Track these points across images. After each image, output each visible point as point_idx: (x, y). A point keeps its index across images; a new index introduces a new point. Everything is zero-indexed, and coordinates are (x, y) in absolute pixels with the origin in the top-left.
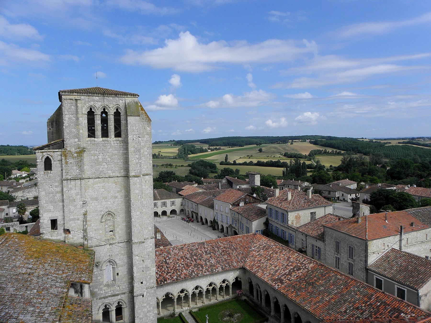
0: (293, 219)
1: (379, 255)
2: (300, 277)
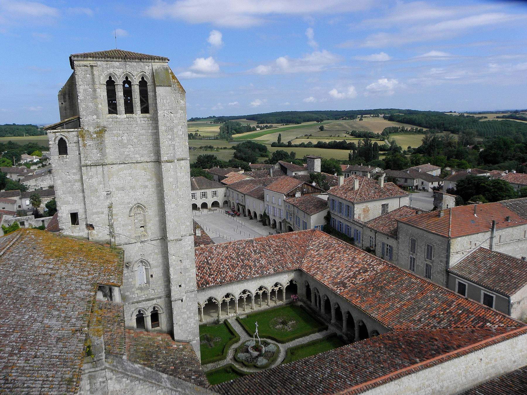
0: (360, 212)
2: (367, 280)
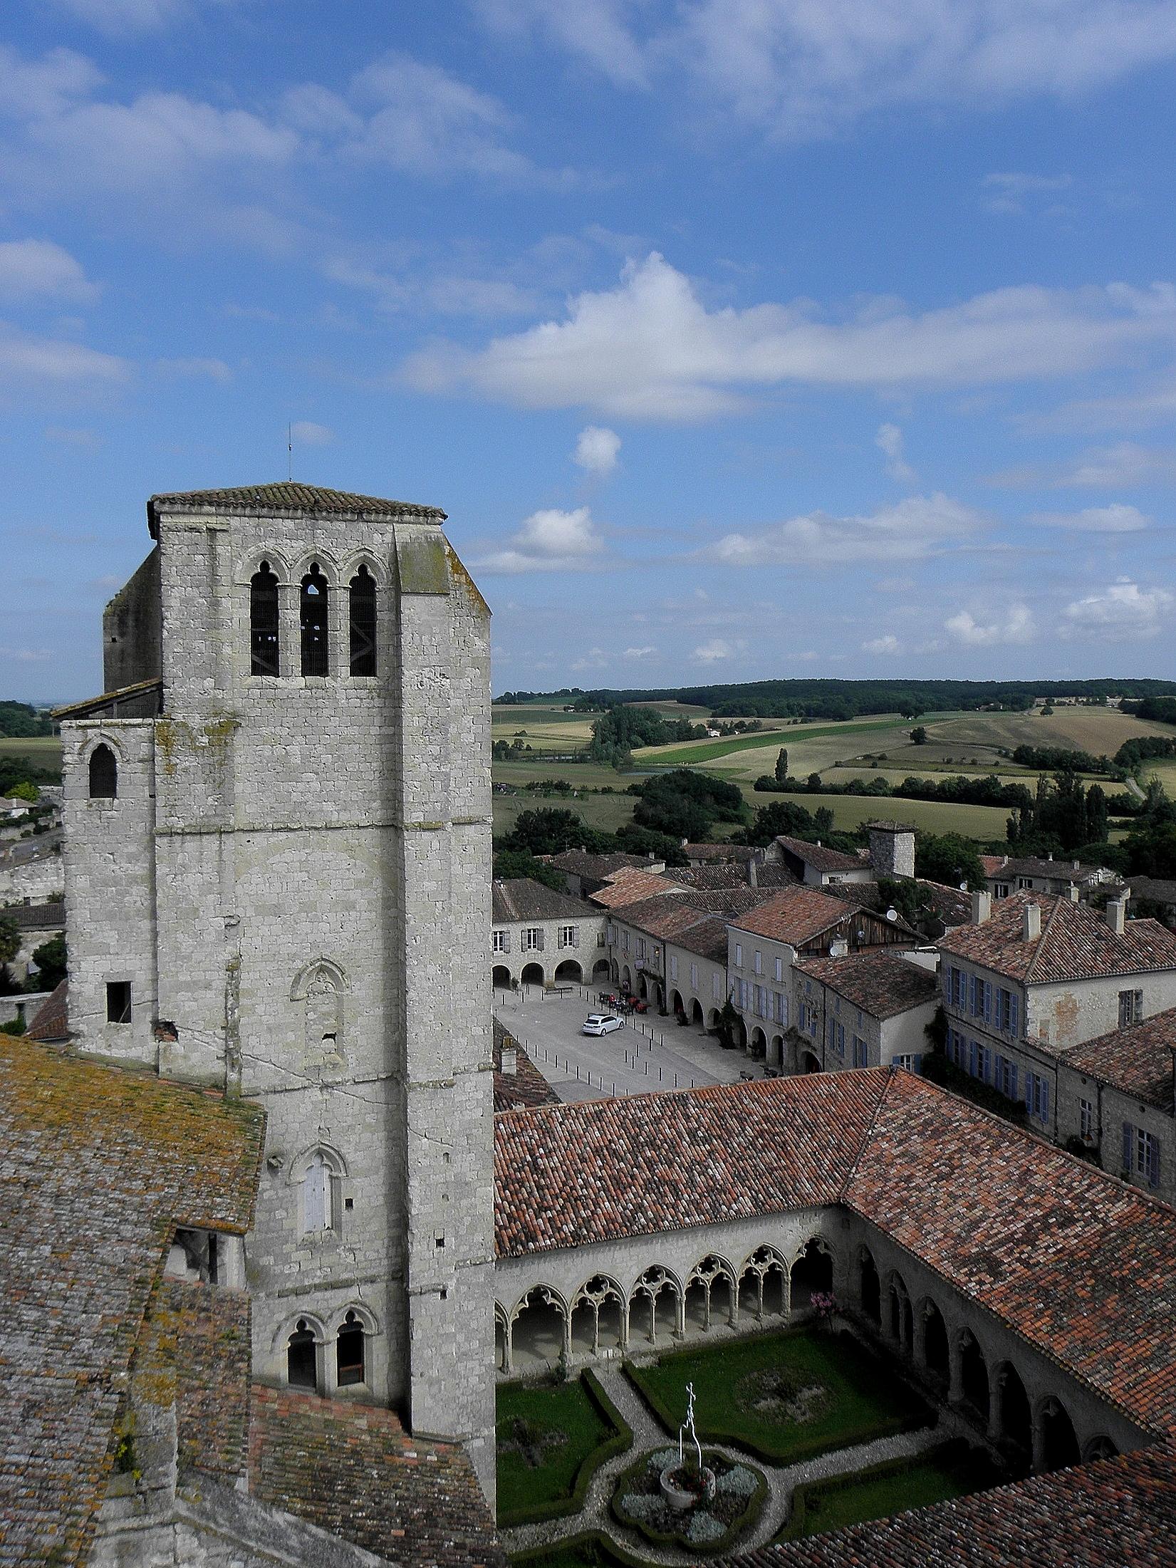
0: (1049, 1016)
2: (1072, 1254)
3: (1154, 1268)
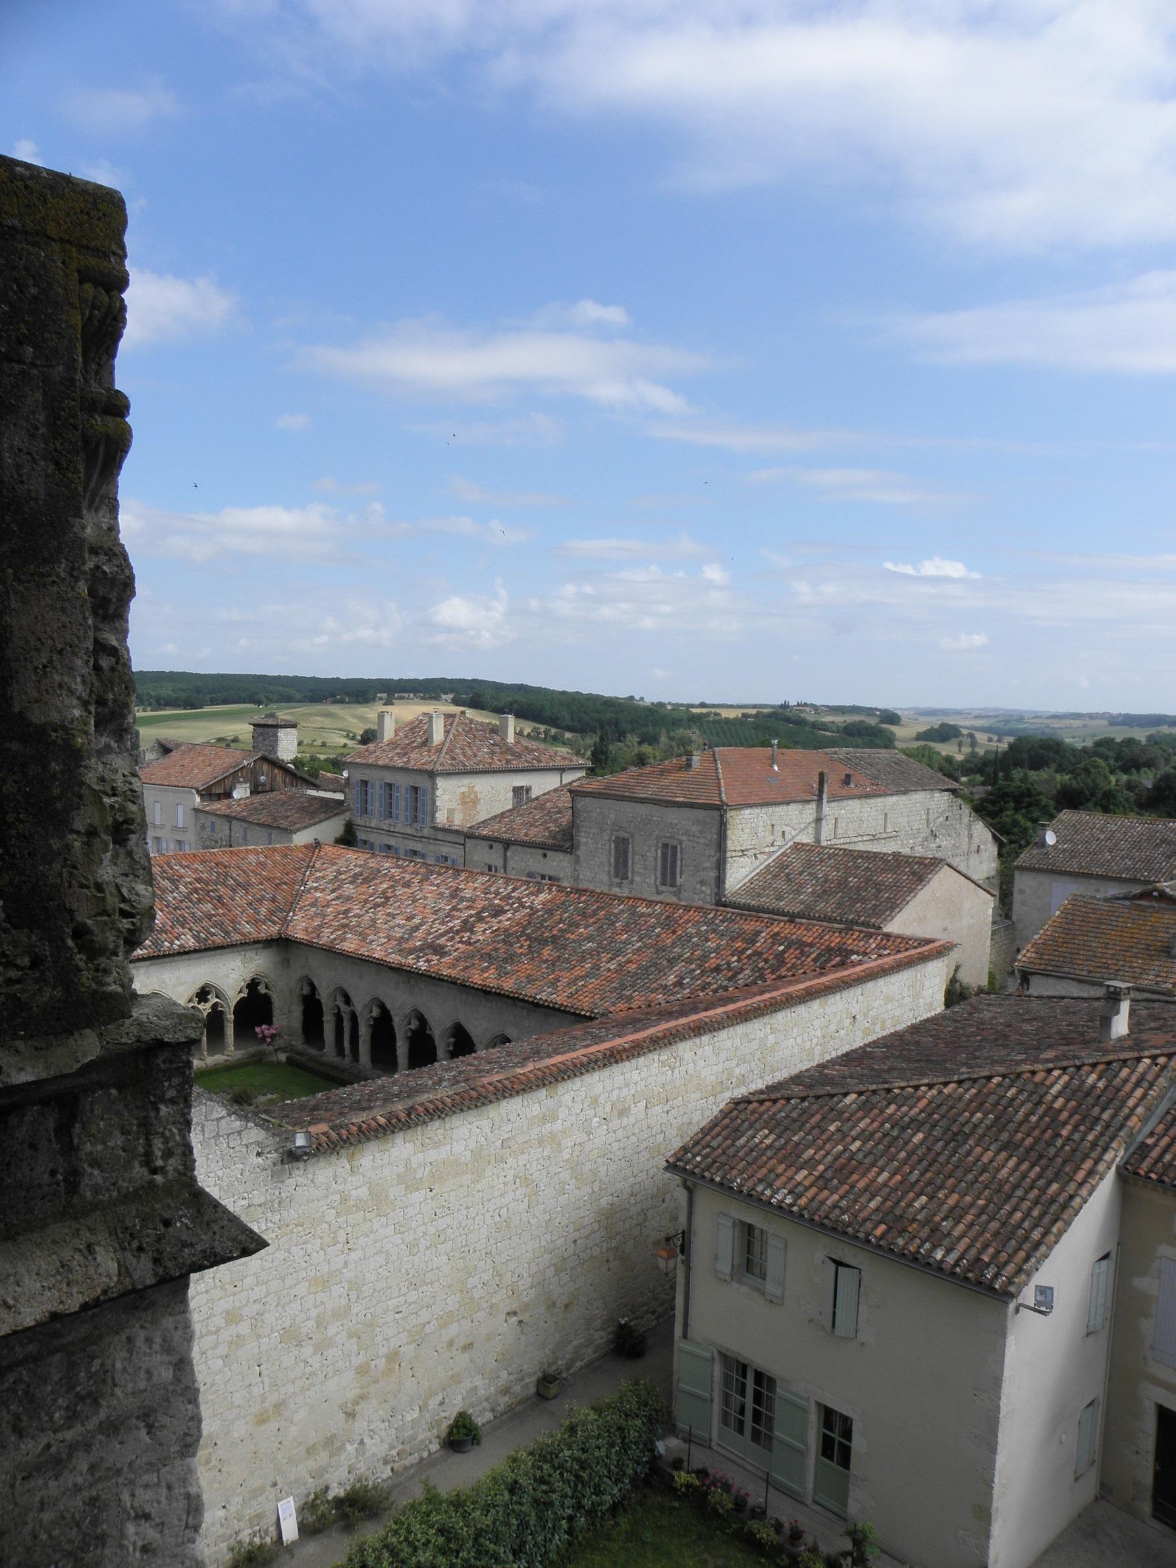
0: (454, 805)
1: (757, 863)
2: (506, 930)
3: (578, 926)
